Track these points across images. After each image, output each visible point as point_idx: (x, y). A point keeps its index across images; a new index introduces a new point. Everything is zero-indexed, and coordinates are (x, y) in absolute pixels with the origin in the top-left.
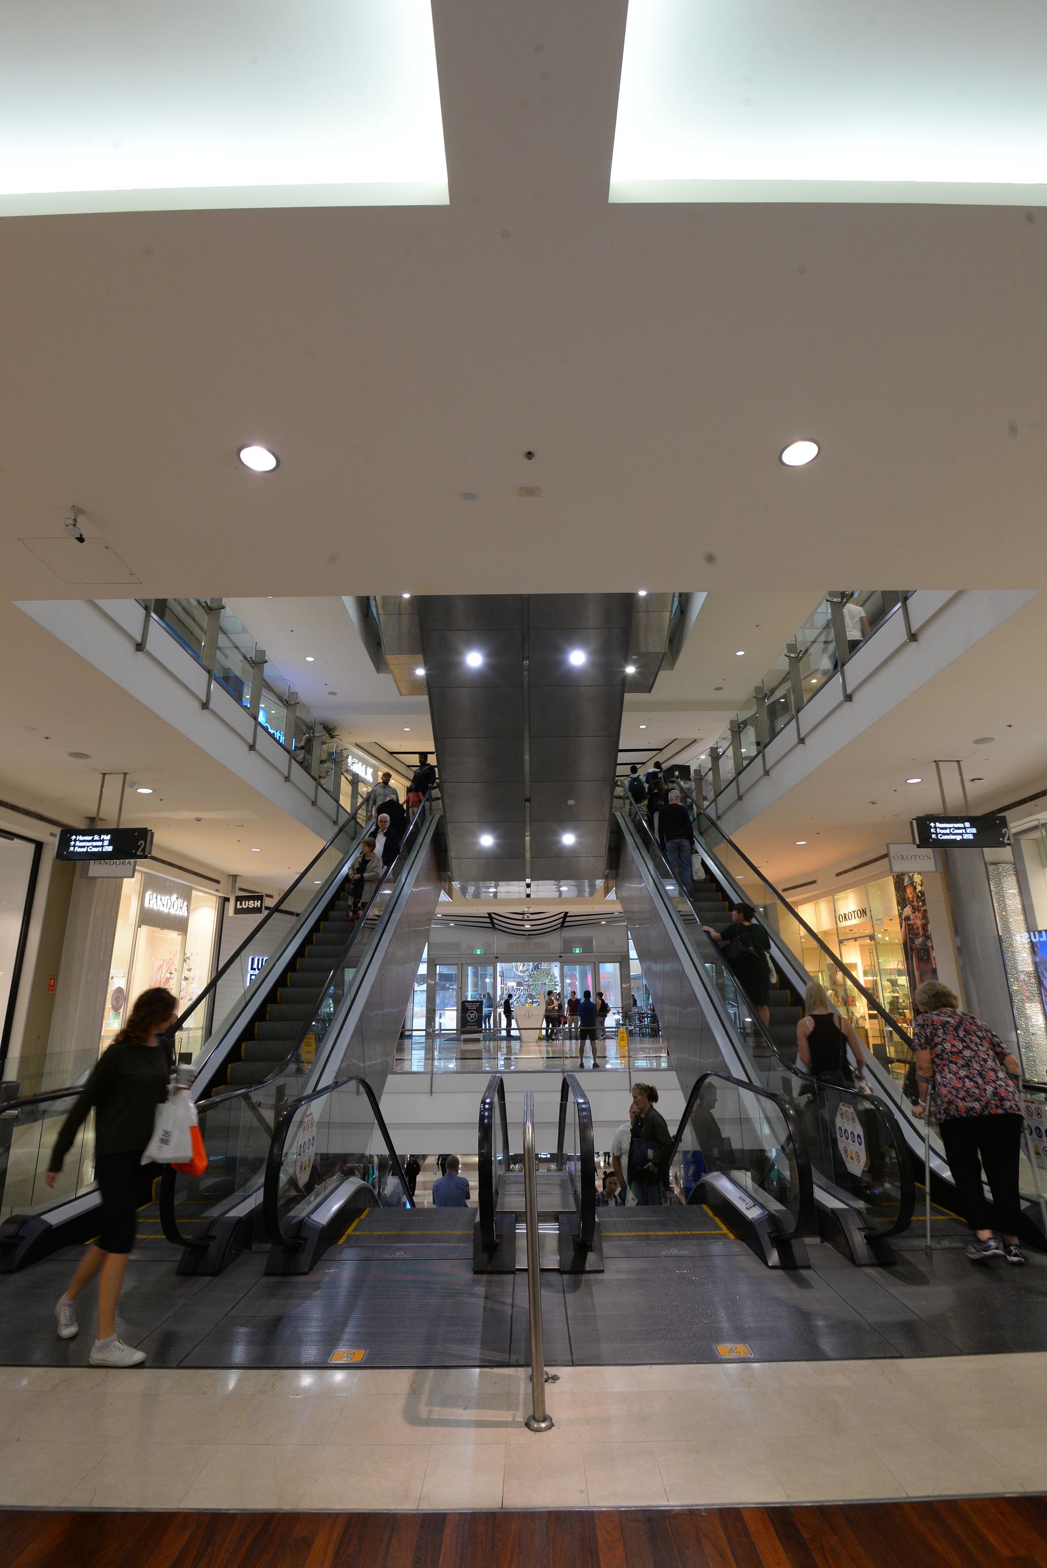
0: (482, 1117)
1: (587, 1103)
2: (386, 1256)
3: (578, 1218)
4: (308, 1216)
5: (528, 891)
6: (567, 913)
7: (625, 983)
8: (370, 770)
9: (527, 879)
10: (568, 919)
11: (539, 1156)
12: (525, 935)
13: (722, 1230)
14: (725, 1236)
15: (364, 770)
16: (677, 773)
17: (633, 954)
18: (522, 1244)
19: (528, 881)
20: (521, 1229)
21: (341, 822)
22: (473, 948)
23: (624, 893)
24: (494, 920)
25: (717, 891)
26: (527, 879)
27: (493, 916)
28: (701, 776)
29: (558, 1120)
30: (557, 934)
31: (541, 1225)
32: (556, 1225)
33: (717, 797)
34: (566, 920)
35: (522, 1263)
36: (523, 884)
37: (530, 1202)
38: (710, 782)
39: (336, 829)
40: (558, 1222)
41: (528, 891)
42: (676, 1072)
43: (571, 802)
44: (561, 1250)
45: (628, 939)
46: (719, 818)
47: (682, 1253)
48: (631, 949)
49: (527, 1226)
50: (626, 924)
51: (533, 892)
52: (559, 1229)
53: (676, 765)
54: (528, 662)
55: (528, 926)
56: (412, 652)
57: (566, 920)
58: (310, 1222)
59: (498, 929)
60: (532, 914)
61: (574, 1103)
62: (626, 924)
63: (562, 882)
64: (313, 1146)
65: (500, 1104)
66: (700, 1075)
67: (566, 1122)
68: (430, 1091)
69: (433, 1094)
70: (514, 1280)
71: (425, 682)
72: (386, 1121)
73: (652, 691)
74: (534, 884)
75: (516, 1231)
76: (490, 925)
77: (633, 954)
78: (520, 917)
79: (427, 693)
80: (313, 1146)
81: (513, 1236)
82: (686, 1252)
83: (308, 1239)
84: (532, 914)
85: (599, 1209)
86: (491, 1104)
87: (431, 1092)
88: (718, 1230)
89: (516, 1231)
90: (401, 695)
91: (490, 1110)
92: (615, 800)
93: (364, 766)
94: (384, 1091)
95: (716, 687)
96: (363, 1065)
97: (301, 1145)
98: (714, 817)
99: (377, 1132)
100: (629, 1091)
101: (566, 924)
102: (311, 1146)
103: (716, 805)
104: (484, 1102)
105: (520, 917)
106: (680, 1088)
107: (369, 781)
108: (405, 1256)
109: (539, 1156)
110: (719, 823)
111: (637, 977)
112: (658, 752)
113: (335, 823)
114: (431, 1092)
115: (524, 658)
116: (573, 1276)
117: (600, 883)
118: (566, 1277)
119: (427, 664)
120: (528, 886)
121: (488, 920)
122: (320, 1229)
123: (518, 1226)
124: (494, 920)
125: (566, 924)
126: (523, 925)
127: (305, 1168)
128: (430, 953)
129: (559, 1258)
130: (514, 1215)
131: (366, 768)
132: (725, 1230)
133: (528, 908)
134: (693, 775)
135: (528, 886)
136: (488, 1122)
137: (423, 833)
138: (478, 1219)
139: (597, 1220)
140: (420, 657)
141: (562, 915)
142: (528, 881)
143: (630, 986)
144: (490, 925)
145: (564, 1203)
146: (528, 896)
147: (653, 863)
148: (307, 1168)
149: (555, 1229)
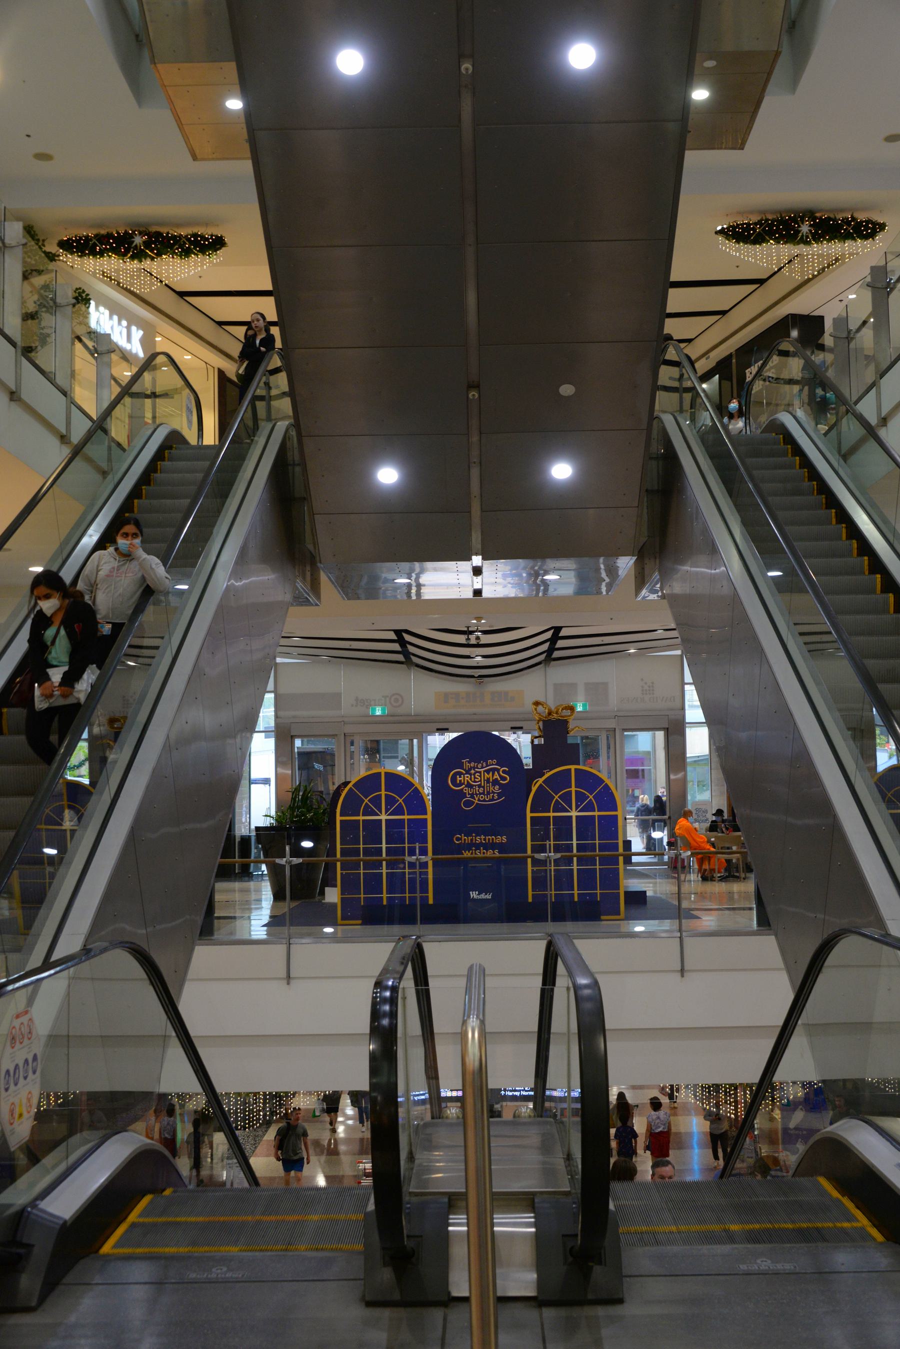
0: (375, 1015)
1: (595, 985)
2: (193, 1275)
3: (574, 1203)
4: (33, 1203)
5: (477, 583)
6: (557, 629)
7: (676, 773)
8: (137, 334)
9: (474, 557)
10: (560, 644)
11: (503, 1093)
12: (472, 677)
13: (858, 1221)
14: (862, 1232)
15: (125, 331)
16: (795, 334)
17: (694, 713)
18: (459, 1253)
19: (477, 560)
20: (458, 1226)
21: (76, 437)
22: (367, 703)
23: (677, 587)
24: (412, 657)
25: (872, 571)
26: (474, 557)
27: (407, 637)
28: (849, 332)
29: (536, 1029)
30: (538, 672)
31: (498, 1218)
32: (529, 1217)
33: (882, 376)
34: (557, 646)
35: (460, 1286)
36: (465, 567)
37: (483, 1174)
38: (866, 353)
39: (66, 451)
40: (534, 1212)
41: (477, 583)
42: (776, 936)
43: (567, 390)
44: (541, 1264)
45: (683, 684)
46: (884, 421)
47: (779, 1266)
48: (691, 707)
49: (468, 1219)
50: (679, 652)
51: (487, 584)
52: (535, 1225)
53: (793, 316)
54: (470, 67)
55: (479, 659)
56: (213, 55)
57: (557, 646)
58: (37, 1215)
59: (418, 666)
60: (485, 632)
61: (568, 989)
62: (679, 652)
63: (551, 563)
64: (34, 1072)
65: (417, 992)
66: (825, 936)
67: (552, 1030)
68: (284, 975)
69: (292, 981)
70: (445, 1319)
71: (243, 120)
72: (192, 1032)
73: (747, 146)
74: (489, 567)
75: (450, 1228)
76: (400, 658)
77: (694, 713)
78: (461, 639)
79: (249, 155)
80: (34, 1072)
81: (445, 1238)
82: (788, 1267)
83: (33, 1246)
84: (485, 632)
85: (616, 1187)
86: (394, 989)
87: (289, 978)
88: (848, 1221)
89: (450, 1228)
90: (195, 158)
91: (393, 1001)
92: (660, 395)
93: (124, 323)
94: (191, 974)
95: (887, 134)
96: (144, 931)
97: (8, 1072)
98: (873, 421)
99: (176, 1053)
100: (679, 974)
101: (556, 654)
102: (21, 1066)
103: (879, 394)
104: (379, 984)
105: (461, 639)
106: (782, 966)
107: (136, 355)
108: (229, 1275)
109: (503, 1093)
110: (882, 433)
111: (698, 761)
112: (756, 286)
113: (64, 439)
114: (289, 978)
115: (461, 57)
116: (562, 1312)
117: (626, 564)
118: (549, 1313)
119: (246, 91)
120: (477, 571)
121: (396, 647)
122: (58, 1227)
123: (453, 1219)
124: (412, 657)
125: (556, 654)
126: (468, 657)
127: (21, 1115)
128: (280, 713)
129: (535, 1276)
130: (446, 1200)
131: (128, 328)
132: (863, 1220)
133: (479, 619)
134: (832, 330)
135: (477, 571)
136: (391, 1024)
137: (250, 465)
138: (371, 1207)
139: (611, 1206)
140: (230, 69)
141: (549, 635)
142: (477, 560)
143: (685, 776)
144: (400, 658)
145: (548, 1173)
146: (478, 593)
147: (738, 517)
148: (25, 1114)
149: (528, 1225)
